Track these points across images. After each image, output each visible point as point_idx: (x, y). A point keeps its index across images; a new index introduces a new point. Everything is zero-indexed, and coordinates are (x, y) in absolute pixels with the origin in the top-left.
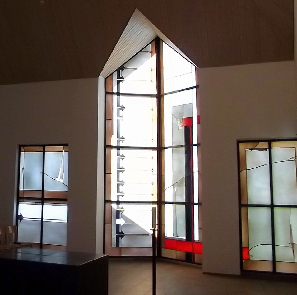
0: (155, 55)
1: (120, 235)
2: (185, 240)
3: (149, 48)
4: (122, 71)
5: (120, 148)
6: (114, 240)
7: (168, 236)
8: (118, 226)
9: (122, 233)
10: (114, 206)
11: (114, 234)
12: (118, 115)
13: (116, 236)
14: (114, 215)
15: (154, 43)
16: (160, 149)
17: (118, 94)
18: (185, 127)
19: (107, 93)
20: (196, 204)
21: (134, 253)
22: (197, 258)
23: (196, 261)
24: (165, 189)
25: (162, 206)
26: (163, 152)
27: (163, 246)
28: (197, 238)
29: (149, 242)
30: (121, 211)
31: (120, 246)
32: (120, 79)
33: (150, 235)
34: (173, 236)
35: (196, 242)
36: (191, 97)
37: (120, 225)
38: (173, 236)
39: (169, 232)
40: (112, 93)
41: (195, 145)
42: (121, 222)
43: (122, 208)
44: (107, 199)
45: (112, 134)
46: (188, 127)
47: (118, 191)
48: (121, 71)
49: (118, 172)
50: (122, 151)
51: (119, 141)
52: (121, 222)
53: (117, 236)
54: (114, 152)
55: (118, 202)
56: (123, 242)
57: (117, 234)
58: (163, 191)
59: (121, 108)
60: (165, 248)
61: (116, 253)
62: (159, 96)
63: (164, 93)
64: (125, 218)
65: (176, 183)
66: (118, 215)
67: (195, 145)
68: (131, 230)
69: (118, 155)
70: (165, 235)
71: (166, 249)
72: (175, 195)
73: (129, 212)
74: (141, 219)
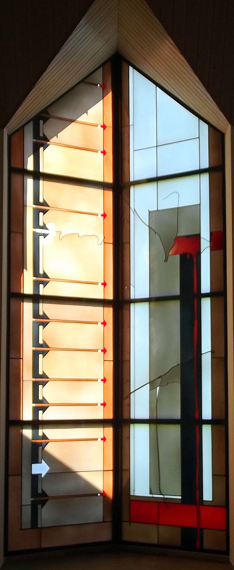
0: (110, 95)
1: (40, 498)
2: (180, 502)
3: (99, 76)
4: (44, 123)
5: (41, 301)
6: (27, 512)
7: (137, 494)
8: (36, 478)
9: (44, 494)
10: (28, 433)
11: (27, 498)
12: (36, 224)
13: (30, 503)
14: (27, 452)
15: (108, 66)
16: (120, 303)
17: (37, 175)
18: (180, 255)
19: (12, 170)
20: (207, 422)
21: (69, 538)
22: (209, 540)
23: (207, 545)
24: (132, 390)
25: (125, 429)
26: (125, 312)
27: (125, 516)
28: (208, 495)
29: (97, 512)
30: (42, 443)
31: (39, 526)
32: (41, 142)
33: (99, 495)
34: (151, 494)
35: (205, 503)
36: (195, 194)
37: (39, 477)
38: (151, 494)
39: (141, 486)
40: (25, 173)
41: (206, 295)
42: (41, 469)
43: (44, 437)
44: (11, 418)
45: (22, 266)
46: (188, 257)
47: (36, 399)
48: (41, 122)
49: (36, 355)
50: (44, 308)
51: (36, 284)
52: (41, 469)
53: (32, 502)
54: (27, 307)
55: (36, 424)
56: (47, 515)
57: (32, 497)
58: (125, 395)
59: (42, 207)
60: (130, 522)
61: (28, 543)
62: (119, 187)
63: (132, 179)
64: (51, 460)
65: (159, 378)
66: (37, 451)
67: (206, 295)
68: (64, 487)
69: (36, 315)
70: (132, 493)
71: (132, 524)
72: (154, 403)
73: (59, 444)
74: (88, 460)
